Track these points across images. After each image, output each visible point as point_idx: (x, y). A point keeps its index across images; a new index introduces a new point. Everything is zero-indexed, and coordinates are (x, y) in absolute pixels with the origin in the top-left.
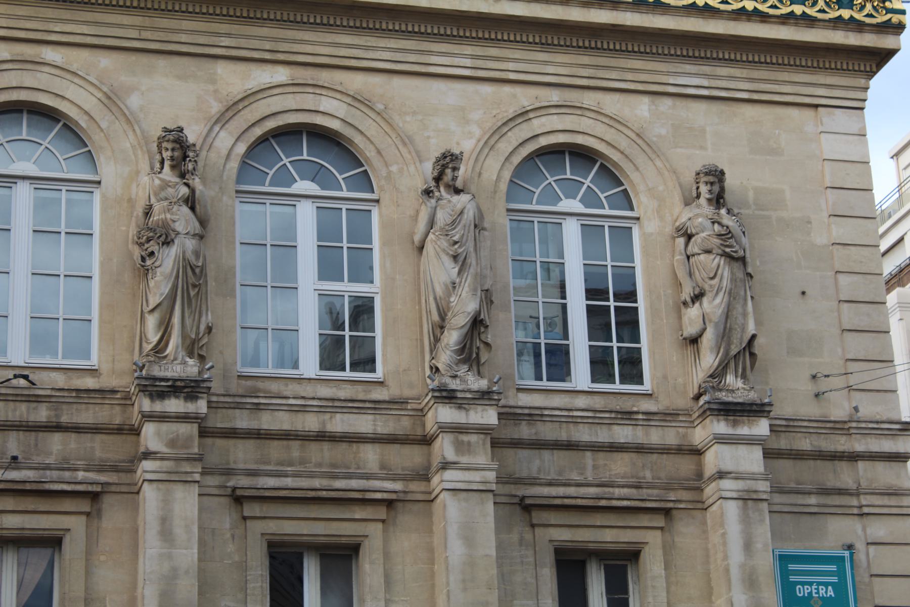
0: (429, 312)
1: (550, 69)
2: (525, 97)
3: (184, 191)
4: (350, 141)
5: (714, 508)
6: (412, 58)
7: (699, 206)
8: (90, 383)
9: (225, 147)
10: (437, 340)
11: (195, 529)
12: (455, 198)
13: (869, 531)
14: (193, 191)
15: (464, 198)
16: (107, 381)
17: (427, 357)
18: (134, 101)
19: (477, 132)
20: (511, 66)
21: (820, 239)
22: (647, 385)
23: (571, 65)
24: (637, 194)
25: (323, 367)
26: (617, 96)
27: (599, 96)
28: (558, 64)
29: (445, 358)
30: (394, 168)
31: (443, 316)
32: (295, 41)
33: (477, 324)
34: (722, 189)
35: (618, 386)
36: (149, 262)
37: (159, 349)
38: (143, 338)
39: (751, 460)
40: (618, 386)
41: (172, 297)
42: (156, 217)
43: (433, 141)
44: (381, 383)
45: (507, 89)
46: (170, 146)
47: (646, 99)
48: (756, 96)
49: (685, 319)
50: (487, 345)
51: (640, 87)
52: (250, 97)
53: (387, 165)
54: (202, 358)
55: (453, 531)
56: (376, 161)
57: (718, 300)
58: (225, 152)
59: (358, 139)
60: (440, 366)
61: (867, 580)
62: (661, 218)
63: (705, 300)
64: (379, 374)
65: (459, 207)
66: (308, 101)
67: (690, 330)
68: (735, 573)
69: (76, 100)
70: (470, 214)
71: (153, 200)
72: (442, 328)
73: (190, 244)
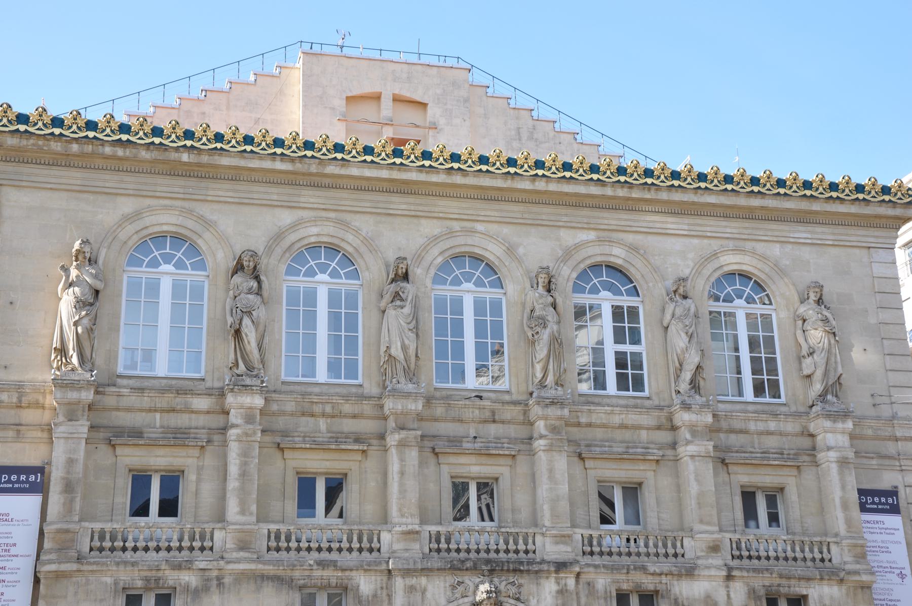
0: (673, 362)
1: (729, 230)
2: (715, 245)
3: (550, 299)
4: (628, 270)
5: (823, 466)
6: (658, 225)
7: (809, 304)
8: (507, 398)
9: (566, 275)
10: (678, 376)
11: (566, 475)
12: (684, 302)
13: (906, 479)
14: (555, 300)
15: (689, 301)
16: (515, 397)
17: (673, 385)
18: (521, 251)
19: (691, 264)
20: (708, 229)
21: (873, 320)
22: (783, 399)
23: (739, 228)
24: (774, 297)
25: (619, 389)
26: (763, 244)
27: (754, 244)
28: (732, 227)
29: (684, 386)
30: (651, 284)
32: (599, 218)
33: (699, 367)
34: (821, 295)
35: (631, 393)
36: (536, 337)
37: (542, 385)
38: (534, 375)
39: (843, 440)
40: (768, 399)
42: (537, 313)
43: (670, 269)
44: (648, 398)
45: (706, 241)
46: (543, 276)
47: (778, 245)
48: (836, 243)
49: (804, 365)
50: (704, 379)
51: (775, 239)
52: (578, 247)
53: (647, 283)
54: (562, 386)
55: (692, 477)
56: (642, 282)
57: (823, 355)
58: (566, 277)
59: (632, 270)
60: (681, 391)
61: (906, 505)
62: (788, 310)
63: (815, 356)
64: (646, 393)
65: (687, 306)
66: (606, 249)
67: (806, 372)
68: (837, 501)
69: (350, 242)
70: (693, 310)
71: (535, 304)
72: (681, 370)
73: (555, 327)
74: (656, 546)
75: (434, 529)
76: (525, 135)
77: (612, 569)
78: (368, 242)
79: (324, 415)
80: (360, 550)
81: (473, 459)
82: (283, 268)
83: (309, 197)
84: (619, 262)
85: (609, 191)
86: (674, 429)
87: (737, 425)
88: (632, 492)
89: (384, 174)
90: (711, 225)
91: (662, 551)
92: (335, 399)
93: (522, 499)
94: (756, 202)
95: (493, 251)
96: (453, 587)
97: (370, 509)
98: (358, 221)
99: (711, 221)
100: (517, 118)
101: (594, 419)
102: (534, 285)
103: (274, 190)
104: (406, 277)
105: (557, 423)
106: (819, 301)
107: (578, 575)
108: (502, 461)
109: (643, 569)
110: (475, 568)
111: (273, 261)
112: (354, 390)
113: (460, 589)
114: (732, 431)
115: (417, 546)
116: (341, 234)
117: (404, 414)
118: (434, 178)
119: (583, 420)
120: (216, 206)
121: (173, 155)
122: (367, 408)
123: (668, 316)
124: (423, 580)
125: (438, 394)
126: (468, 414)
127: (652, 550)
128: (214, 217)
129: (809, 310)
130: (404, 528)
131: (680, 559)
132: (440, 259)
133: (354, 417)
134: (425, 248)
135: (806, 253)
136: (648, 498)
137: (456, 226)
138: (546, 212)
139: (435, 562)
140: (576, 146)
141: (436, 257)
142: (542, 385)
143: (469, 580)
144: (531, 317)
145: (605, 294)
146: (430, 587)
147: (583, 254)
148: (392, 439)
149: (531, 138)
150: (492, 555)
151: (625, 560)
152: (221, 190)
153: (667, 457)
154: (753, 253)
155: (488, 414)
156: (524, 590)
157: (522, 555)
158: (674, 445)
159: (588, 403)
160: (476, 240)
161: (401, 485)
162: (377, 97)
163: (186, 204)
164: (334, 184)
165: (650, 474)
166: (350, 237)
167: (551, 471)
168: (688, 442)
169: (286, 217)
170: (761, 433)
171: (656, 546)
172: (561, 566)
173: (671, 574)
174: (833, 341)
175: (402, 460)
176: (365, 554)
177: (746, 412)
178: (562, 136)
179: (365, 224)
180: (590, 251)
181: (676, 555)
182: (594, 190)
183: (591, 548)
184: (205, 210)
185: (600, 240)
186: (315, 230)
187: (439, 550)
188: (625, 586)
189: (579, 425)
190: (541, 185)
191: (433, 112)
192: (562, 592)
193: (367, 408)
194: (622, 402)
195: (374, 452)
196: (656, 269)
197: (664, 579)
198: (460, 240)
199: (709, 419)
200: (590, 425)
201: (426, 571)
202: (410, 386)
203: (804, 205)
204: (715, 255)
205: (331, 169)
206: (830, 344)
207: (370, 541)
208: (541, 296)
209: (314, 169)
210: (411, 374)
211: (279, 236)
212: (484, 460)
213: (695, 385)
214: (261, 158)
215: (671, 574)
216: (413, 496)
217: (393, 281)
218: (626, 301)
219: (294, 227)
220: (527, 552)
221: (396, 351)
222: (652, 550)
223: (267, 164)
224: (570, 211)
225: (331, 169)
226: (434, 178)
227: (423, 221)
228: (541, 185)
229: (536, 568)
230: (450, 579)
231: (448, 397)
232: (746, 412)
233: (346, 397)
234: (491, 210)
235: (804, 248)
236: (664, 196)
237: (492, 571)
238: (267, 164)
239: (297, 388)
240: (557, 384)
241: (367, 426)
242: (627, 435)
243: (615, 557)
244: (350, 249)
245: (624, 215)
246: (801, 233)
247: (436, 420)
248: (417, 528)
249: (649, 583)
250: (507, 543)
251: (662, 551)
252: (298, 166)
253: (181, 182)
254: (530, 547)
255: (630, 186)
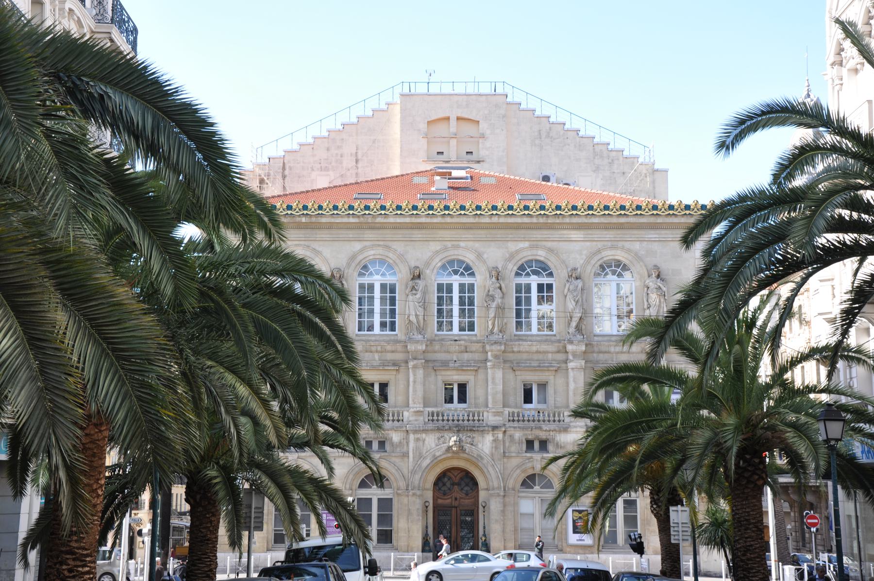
3: (498, 285)
15: (579, 281)
18: (485, 256)
28: (610, 234)
29: (572, 330)
31: (571, 318)
37: (492, 332)
41: (495, 317)
45: (594, 243)
52: (517, 252)
66: (534, 252)
73: (500, 301)
74: (549, 416)
75: (430, 409)
76: (544, 135)
77: (523, 429)
78: (401, 257)
79: (377, 351)
80: (393, 421)
81: (454, 372)
82: (356, 274)
83: (369, 234)
84: (542, 259)
85: (534, 220)
86: (566, 352)
87: (603, 349)
88: (543, 386)
89: (408, 220)
90: (597, 234)
91: (552, 419)
92: (382, 344)
93: (480, 392)
94: (623, 220)
95: (469, 258)
96: (439, 439)
97: (401, 399)
98: (395, 245)
99: (598, 232)
100: (539, 124)
101: (522, 349)
102: (491, 276)
103: (350, 232)
104: (419, 277)
105: (498, 353)
106: (658, 276)
107: (505, 432)
108: (470, 373)
109: (540, 428)
110: (450, 429)
111: (350, 271)
112: (392, 338)
113: (442, 439)
114: (600, 352)
115: (422, 418)
116: (386, 253)
117: (416, 351)
118: (435, 220)
119: (515, 349)
120: (321, 243)
121: (298, 219)
122: (399, 347)
123: (566, 290)
124: (424, 435)
125: (437, 338)
126: (452, 349)
127: (547, 418)
128: (320, 249)
129: (652, 283)
130: (415, 409)
131: (562, 423)
132: (440, 264)
133: (393, 352)
134: (432, 258)
135: (656, 246)
136: (550, 390)
137: (449, 244)
138: (500, 233)
139: (431, 426)
140: (578, 139)
141: (437, 263)
142: (492, 332)
143: (446, 435)
144: (488, 295)
145: (534, 277)
146: (427, 439)
147: (521, 255)
148: (411, 364)
149: (548, 136)
150: (461, 422)
151: (532, 424)
152: (323, 234)
153: (560, 368)
154: (623, 248)
155: (463, 348)
156: (476, 440)
157: (476, 422)
158: (566, 362)
159: (519, 340)
160: (460, 252)
161: (414, 387)
162: (448, 118)
163: (306, 243)
164: (382, 227)
165: (552, 377)
166: (391, 255)
167: (493, 379)
168: (571, 361)
169: (357, 246)
170: (618, 353)
171: (549, 416)
172: (495, 428)
173: (555, 430)
174: (662, 300)
175: (415, 375)
176: (396, 422)
177: (611, 341)
178: (569, 133)
179: (399, 247)
180: (525, 254)
181: (559, 421)
182: (526, 220)
183: (513, 419)
184: (315, 245)
185: (531, 247)
186: (372, 252)
187: (433, 420)
188: (530, 437)
189: (513, 352)
190: (495, 220)
191: (483, 126)
192: (495, 441)
193: (399, 347)
194: (538, 338)
195: (402, 369)
196: (563, 262)
197: (551, 433)
198: (451, 253)
199: (583, 348)
200: (519, 352)
201: (425, 431)
202: (420, 336)
203: (652, 220)
204: (599, 251)
205: (380, 220)
206: (660, 301)
207: (398, 416)
208: (493, 283)
209: (370, 220)
210: (421, 330)
211: (353, 258)
212: (460, 372)
213: (578, 329)
214: (342, 217)
215: (555, 430)
216: (420, 393)
217: (412, 279)
218: (546, 280)
219: (362, 251)
220: (479, 420)
221: (413, 318)
222: (547, 418)
223: (345, 220)
224: (513, 231)
225: (380, 220)
226: (435, 220)
227: (431, 243)
228: (495, 220)
229: (481, 429)
230: (438, 435)
231: (442, 340)
232: (611, 341)
233: (388, 342)
234: (469, 234)
235: (656, 244)
236: (567, 220)
237: (459, 431)
238: (345, 220)
239: (363, 338)
240: (501, 331)
241: (399, 356)
242: (540, 357)
243: (526, 422)
244: (391, 261)
245: (545, 232)
246: (652, 235)
247: (435, 352)
248: (422, 409)
249: (543, 435)
250: (468, 416)
251: (552, 419)
252: (362, 219)
253: (303, 231)
254: (481, 418)
255: (547, 216)
